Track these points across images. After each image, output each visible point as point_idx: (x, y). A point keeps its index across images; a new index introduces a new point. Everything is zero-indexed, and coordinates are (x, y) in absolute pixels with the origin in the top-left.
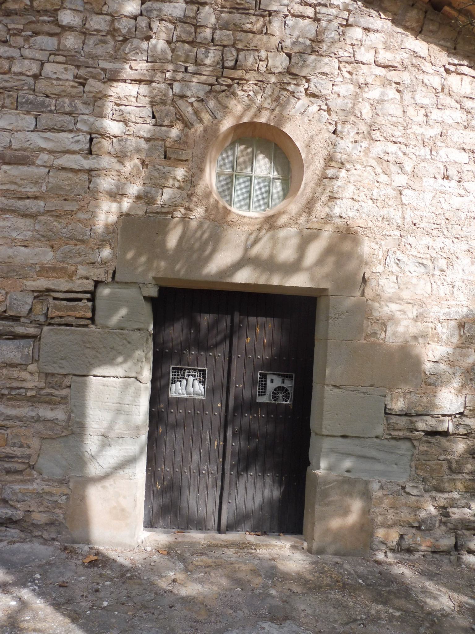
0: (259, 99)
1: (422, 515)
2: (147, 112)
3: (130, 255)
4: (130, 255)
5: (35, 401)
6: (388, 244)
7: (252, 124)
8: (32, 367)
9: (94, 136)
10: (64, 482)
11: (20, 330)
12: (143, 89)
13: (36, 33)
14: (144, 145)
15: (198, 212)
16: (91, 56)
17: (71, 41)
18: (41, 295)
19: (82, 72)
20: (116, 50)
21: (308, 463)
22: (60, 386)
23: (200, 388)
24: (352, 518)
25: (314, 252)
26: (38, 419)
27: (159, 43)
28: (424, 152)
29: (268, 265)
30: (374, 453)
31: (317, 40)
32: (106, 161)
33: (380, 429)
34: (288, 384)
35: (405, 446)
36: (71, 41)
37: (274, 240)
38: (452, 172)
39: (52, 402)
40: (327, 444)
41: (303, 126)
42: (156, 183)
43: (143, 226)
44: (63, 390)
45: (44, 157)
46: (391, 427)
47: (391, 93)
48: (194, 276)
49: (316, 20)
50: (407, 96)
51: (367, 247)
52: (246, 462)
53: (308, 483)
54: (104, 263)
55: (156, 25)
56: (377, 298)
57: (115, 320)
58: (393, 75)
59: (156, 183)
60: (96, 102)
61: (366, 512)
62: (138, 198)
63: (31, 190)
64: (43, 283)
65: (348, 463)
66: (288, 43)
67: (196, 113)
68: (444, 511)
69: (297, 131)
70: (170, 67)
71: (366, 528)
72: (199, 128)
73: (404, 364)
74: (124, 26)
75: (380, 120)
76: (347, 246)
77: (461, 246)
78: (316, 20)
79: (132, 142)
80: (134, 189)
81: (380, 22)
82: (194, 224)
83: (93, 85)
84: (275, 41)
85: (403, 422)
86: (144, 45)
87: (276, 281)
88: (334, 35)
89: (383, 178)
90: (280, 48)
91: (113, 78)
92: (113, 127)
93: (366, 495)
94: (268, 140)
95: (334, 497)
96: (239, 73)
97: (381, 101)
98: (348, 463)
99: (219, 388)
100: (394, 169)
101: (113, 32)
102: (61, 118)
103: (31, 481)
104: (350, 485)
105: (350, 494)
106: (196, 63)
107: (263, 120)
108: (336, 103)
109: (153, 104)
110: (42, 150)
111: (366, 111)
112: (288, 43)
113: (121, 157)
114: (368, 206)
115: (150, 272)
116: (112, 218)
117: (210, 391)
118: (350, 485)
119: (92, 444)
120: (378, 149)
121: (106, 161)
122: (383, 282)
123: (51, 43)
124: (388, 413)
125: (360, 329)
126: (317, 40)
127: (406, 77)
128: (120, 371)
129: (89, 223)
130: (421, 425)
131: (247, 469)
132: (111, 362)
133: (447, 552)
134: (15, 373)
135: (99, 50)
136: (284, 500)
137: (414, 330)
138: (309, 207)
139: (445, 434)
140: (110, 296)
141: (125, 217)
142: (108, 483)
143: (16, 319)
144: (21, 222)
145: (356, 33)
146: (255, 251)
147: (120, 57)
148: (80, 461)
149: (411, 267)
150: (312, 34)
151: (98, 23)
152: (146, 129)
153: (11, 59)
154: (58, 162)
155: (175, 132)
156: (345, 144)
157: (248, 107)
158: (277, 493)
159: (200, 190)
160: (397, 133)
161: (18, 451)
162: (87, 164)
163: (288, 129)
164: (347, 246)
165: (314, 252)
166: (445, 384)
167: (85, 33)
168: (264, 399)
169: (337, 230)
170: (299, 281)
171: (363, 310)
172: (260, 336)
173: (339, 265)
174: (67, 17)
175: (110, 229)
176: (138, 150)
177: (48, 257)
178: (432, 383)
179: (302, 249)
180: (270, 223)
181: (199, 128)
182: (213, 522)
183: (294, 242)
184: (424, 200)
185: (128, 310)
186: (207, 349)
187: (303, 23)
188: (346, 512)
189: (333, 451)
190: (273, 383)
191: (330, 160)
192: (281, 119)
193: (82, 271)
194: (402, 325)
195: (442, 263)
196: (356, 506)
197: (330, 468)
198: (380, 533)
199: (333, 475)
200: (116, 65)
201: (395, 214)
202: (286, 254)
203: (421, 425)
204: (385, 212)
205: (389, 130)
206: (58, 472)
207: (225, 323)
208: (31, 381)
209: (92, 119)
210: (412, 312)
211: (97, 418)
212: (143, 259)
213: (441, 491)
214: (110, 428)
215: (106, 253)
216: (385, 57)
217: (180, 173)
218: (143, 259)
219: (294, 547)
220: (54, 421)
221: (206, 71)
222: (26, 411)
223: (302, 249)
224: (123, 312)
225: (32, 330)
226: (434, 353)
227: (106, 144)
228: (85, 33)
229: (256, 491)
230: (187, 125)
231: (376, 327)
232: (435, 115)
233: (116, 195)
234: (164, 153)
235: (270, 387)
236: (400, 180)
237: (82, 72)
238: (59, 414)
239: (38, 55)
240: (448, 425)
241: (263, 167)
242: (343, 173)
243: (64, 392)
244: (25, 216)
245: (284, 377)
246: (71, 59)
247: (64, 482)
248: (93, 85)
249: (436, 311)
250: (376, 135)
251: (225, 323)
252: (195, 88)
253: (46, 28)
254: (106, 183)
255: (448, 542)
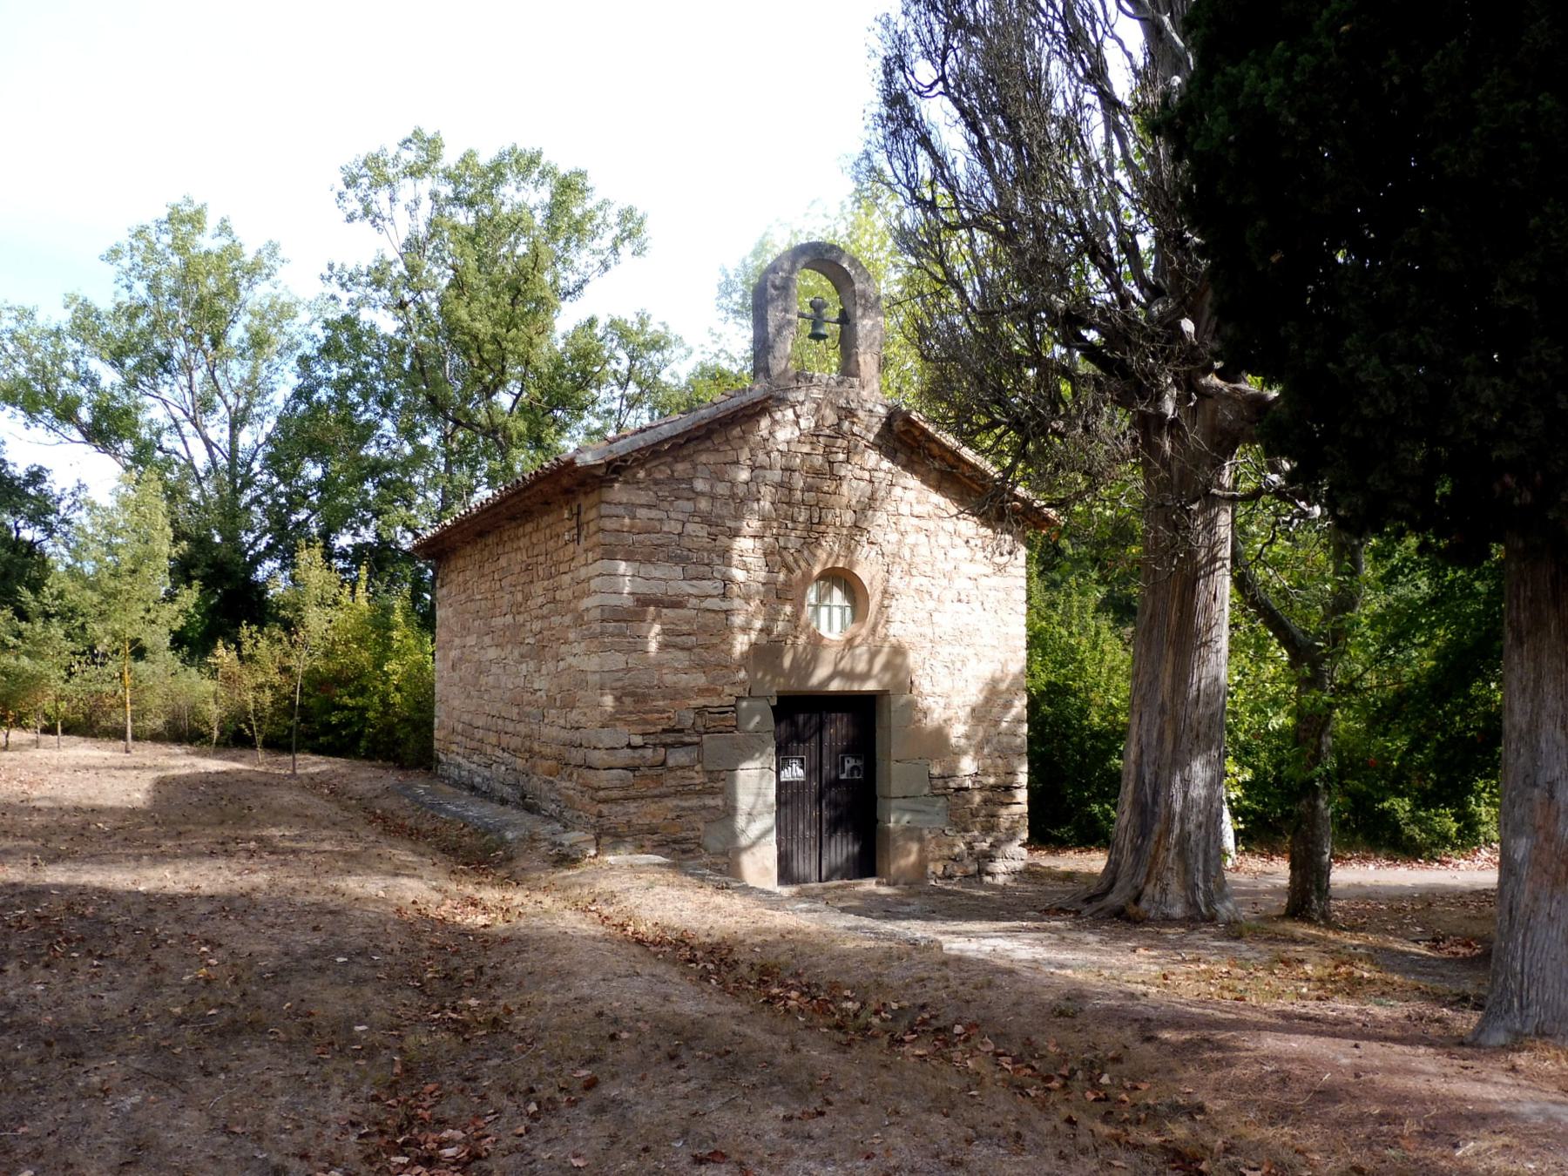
0: (836, 548)
1: (957, 850)
2: (762, 562)
3: (759, 675)
4: (759, 675)
5: (699, 793)
6: (925, 653)
7: (833, 568)
8: (698, 767)
9: (727, 581)
10: (725, 854)
11: (687, 739)
12: (758, 543)
13: (677, 498)
14: (762, 589)
15: (802, 639)
16: (719, 516)
17: (703, 504)
18: (700, 711)
19: (713, 530)
20: (736, 509)
21: (877, 821)
22: (718, 780)
23: (800, 772)
24: (913, 858)
25: (880, 661)
26: (704, 807)
27: (766, 504)
28: (945, 582)
29: (850, 675)
30: (923, 807)
31: (872, 498)
32: (737, 603)
33: (926, 790)
34: (859, 763)
35: (942, 801)
36: (703, 504)
37: (853, 657)
38: (963, 597)
39: (712, 793)
40: (894, 803)
41: (866, 571)
42: (772, 618)
43: (766, 653)
44: (720, 784)
45: (693, 601)
46: (933, 787)
47: (922, 538)
48: (803, 688)
49: (871, 481)
50: (933, 539)
51: (913, 659)
52: (835, 825)
53: (879, 836)
54: (743, 682)
55: (763, 489)
56: (920, 694)
57: (752, 726)
58: (923, 524)
59: (772, 618)
60: (725, 554)
61: (922, 850)
62: (761, 630)
63: (685, 628)
64: (700, 702)
65: (907, 818)
66: (854, 502)
67: (796, 561)
68: (970, 846)
69: (863, 572)
70: (775, 524)
71: (922, 864)
72: (798, 573)
73: (938, 741)
74: (741, 491)
75: (916, 560)
76: (898, 660)
77: (970, 652)
78: (871, 481)
79: (755, 586)
80: (758, 624)
81: (913, 482)
82: (800, 648)
83: (723, 540)
84: (845, 501)
85: (940, 783)
86: (756, 506)
87: (856, 687)
88: (883, 493)
89: (920, 605)
90: (848, 507)
91: (735, 533)
92: (739, 575)
93: (921, 840)
94: (844, 580)
95: (901, 843)
96: (823, 528)
97: (915, 545)
98: (907, 818)
99: (813, 771)
100: (926, 596)
101: (733, 496)
102: (702, 568)
103: (700, 857)
104: (912, 833)
105: (911, 839)
106: (794, 521)
107: (841, 565)
108: (888, 549)
109: (765, 555)
110: (690, 595)
111: (906, 552)
112: (854, 502)
113: (747, 598)
114: (911, 626)
115: (775, 686)
116: (746, 648)
117: (808, 774)
118: (912, 833)
119: (741, 821)
120: (916, 581)
121: (737, 603)
122: (923, 683)
123: (689, 506)
124: (931, 777)
125: (911, 719)
126: (872, 498)
127: (931, 525)
128: (757, 764)
129: (729, 652)
130: (952, 785)
131: (835, 832)
132: (750, 757)
133: (973, 876)
134: (687, 774)
135: (724, 512)
136: (861, 852)
137: (944, 716)
138: (874, 630)
139: (967, 789)
140: (748, 707)
141: (753, 645)
142: (755, 850)
143: (681, 731)
144: (681, 655)
145: (897, 491)
146: (841, 666)
147: (739, 517)
148: (734, 836)
149: (939, 668)
150: (868, 494)
151: (722, 489)
152: (762, 575)
153: (660, 520)
154: (704, 605)
155: (782, 577)
156: (894, 580)
157: (830, 555)
158: (857, 848)
159: (802, 622)
160: (928, 569)
161: (691, 834)
162: (725, 605)
163: (858, 571)
164: (898, 660)
165: (880, 661)
166: (965, 753)
167: (713, 497)
168: (843, 777)
169: (892, 646)
170: (870, 686)
171: (912, 705)
172: (838, 729)
173: (895, 676)
174: (700, 485)
175: (745, 656)
176: (758, 593)
177: (701, 680)
178: (959, 753)
179: (871, 662)
180: (850, 643)
181: (798, 573)
182: (815, 876)
183: (865, 657)
184: (946, 621)
185: (758, 719)
186: (804, 742)
187: (863, 484)
188: (909, 854)
189: (899, 809)
190: (849, 764)
191: (885, 592)
192: (852, 563)
193: (727, 690)
194: (937, 715)
195: (958, 665)
196: (915, 847)
197: (897, 822)
198: (931, 867)
199: (899, 827)
200: (737, 524)
201: (928, 631)
202: (861, 667)
203: (952, 785)
204: (922, 630)
205: (923, 568)
206: (719, 847)
207: (815, 720)
208: (699, 779)
209: (724, 569)
210: (942, 702)
211: (744, 800)
212: (768, 678)
213: (967, 831)
214: (753, 808)
215: (742, 674)
216: (917, 510)
217: (788, 609)
218: (768, 678)
219: (878, 883)
220: (716, 807)
221: (800, 527)
222: (694, 802)
223: (871, 662)
224: (757, 719)
225: (696, 739)
226: (957, 732)
227: (735, 588)
228: (713, 497)
229: (841, 850)
230: (790, 571)
231: (921, 715)
232: (952, 553)
233: (745, 629)
234: (780, 593)
235: (847, 766)
236: (931, 605)
237: (713, 530)
238: (719, 802)
239: (680, 517)
240: (968, 783)
241: (838, 596)
242: (894, 603)
243: (720, 784)
244: (683, 649)
245: (856, 758)
246: (706, 520)
247: (725, 854)
248: (723, 540)
249: (957, 701)
250: (914, 572)
251: (815, 720)
252: (793, 541)
253: (685, 494)
254: (738, 620)
255: (973, 868)
